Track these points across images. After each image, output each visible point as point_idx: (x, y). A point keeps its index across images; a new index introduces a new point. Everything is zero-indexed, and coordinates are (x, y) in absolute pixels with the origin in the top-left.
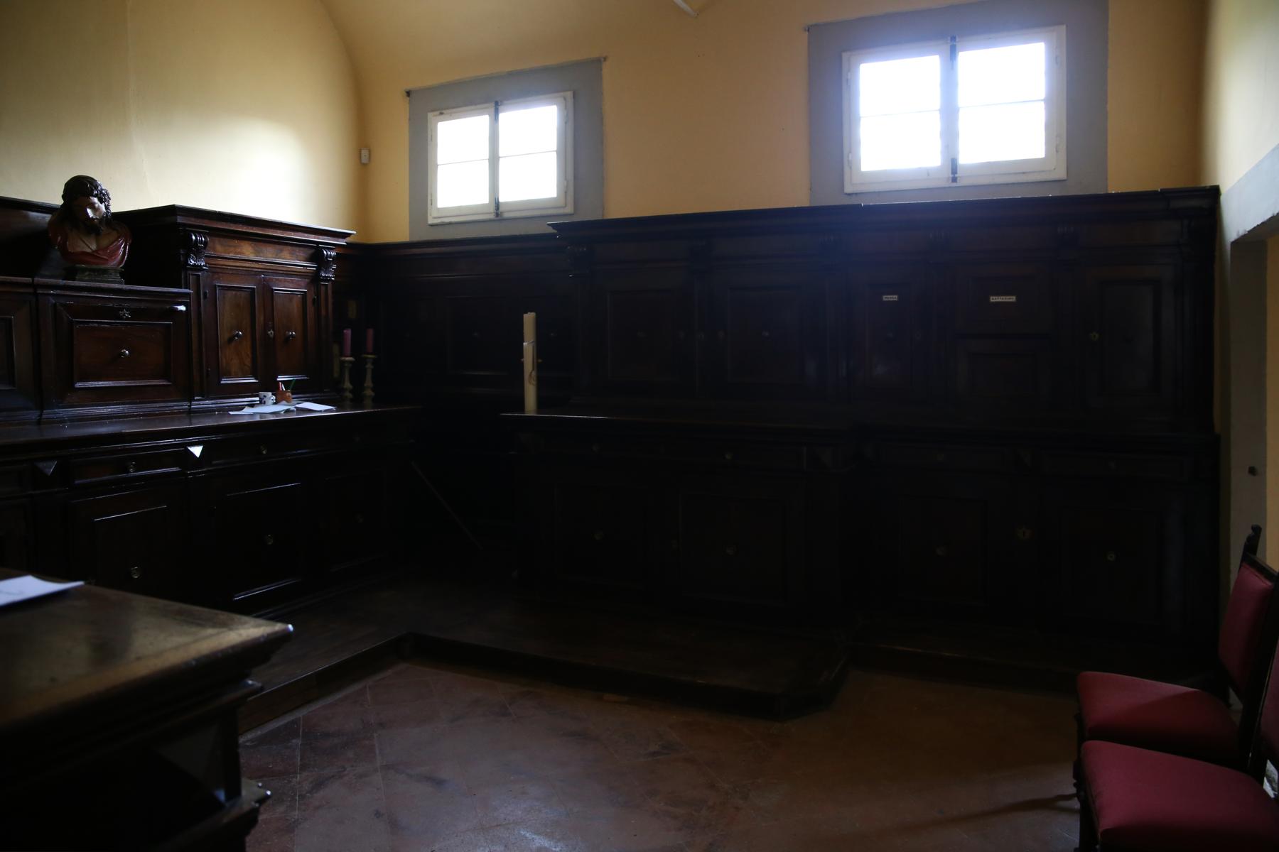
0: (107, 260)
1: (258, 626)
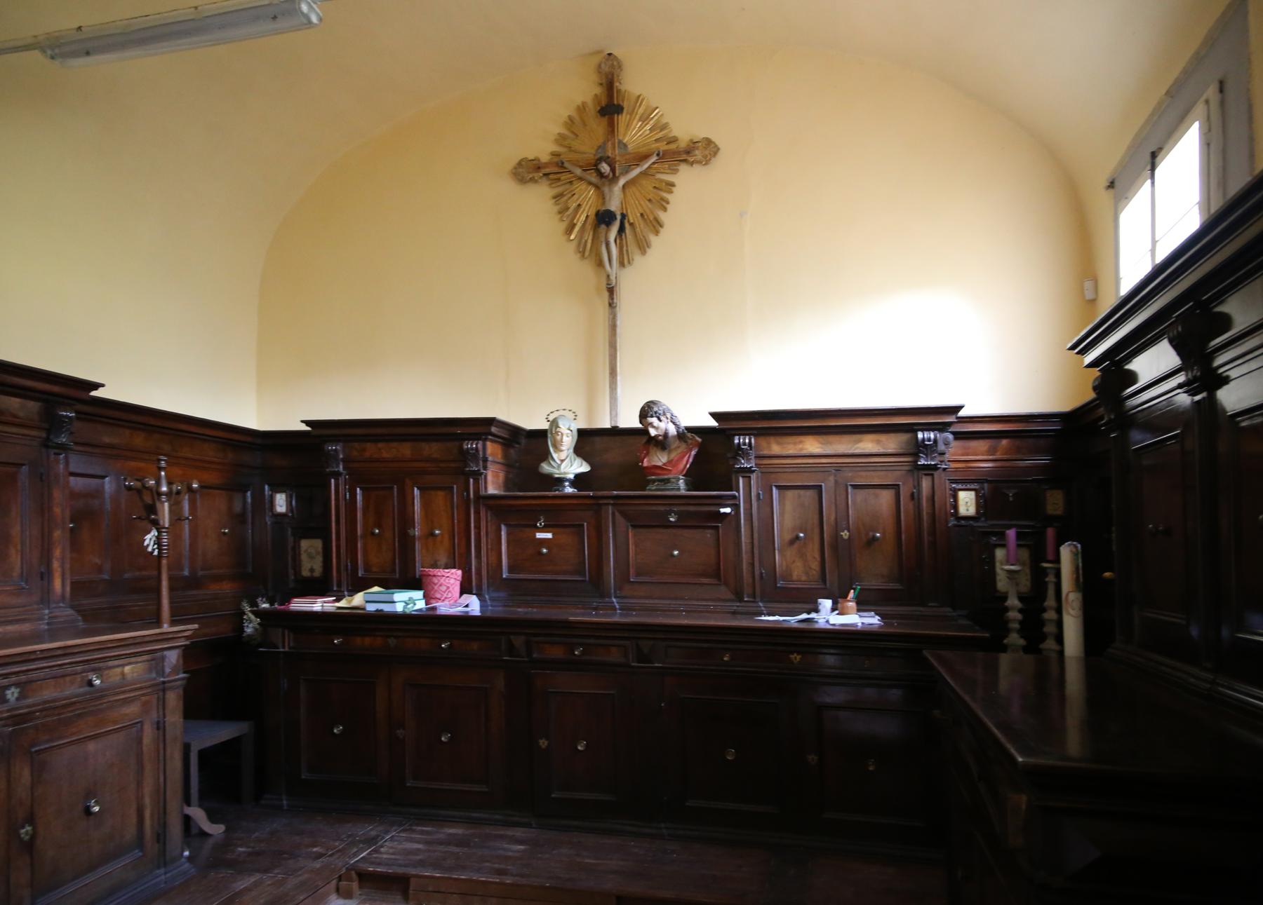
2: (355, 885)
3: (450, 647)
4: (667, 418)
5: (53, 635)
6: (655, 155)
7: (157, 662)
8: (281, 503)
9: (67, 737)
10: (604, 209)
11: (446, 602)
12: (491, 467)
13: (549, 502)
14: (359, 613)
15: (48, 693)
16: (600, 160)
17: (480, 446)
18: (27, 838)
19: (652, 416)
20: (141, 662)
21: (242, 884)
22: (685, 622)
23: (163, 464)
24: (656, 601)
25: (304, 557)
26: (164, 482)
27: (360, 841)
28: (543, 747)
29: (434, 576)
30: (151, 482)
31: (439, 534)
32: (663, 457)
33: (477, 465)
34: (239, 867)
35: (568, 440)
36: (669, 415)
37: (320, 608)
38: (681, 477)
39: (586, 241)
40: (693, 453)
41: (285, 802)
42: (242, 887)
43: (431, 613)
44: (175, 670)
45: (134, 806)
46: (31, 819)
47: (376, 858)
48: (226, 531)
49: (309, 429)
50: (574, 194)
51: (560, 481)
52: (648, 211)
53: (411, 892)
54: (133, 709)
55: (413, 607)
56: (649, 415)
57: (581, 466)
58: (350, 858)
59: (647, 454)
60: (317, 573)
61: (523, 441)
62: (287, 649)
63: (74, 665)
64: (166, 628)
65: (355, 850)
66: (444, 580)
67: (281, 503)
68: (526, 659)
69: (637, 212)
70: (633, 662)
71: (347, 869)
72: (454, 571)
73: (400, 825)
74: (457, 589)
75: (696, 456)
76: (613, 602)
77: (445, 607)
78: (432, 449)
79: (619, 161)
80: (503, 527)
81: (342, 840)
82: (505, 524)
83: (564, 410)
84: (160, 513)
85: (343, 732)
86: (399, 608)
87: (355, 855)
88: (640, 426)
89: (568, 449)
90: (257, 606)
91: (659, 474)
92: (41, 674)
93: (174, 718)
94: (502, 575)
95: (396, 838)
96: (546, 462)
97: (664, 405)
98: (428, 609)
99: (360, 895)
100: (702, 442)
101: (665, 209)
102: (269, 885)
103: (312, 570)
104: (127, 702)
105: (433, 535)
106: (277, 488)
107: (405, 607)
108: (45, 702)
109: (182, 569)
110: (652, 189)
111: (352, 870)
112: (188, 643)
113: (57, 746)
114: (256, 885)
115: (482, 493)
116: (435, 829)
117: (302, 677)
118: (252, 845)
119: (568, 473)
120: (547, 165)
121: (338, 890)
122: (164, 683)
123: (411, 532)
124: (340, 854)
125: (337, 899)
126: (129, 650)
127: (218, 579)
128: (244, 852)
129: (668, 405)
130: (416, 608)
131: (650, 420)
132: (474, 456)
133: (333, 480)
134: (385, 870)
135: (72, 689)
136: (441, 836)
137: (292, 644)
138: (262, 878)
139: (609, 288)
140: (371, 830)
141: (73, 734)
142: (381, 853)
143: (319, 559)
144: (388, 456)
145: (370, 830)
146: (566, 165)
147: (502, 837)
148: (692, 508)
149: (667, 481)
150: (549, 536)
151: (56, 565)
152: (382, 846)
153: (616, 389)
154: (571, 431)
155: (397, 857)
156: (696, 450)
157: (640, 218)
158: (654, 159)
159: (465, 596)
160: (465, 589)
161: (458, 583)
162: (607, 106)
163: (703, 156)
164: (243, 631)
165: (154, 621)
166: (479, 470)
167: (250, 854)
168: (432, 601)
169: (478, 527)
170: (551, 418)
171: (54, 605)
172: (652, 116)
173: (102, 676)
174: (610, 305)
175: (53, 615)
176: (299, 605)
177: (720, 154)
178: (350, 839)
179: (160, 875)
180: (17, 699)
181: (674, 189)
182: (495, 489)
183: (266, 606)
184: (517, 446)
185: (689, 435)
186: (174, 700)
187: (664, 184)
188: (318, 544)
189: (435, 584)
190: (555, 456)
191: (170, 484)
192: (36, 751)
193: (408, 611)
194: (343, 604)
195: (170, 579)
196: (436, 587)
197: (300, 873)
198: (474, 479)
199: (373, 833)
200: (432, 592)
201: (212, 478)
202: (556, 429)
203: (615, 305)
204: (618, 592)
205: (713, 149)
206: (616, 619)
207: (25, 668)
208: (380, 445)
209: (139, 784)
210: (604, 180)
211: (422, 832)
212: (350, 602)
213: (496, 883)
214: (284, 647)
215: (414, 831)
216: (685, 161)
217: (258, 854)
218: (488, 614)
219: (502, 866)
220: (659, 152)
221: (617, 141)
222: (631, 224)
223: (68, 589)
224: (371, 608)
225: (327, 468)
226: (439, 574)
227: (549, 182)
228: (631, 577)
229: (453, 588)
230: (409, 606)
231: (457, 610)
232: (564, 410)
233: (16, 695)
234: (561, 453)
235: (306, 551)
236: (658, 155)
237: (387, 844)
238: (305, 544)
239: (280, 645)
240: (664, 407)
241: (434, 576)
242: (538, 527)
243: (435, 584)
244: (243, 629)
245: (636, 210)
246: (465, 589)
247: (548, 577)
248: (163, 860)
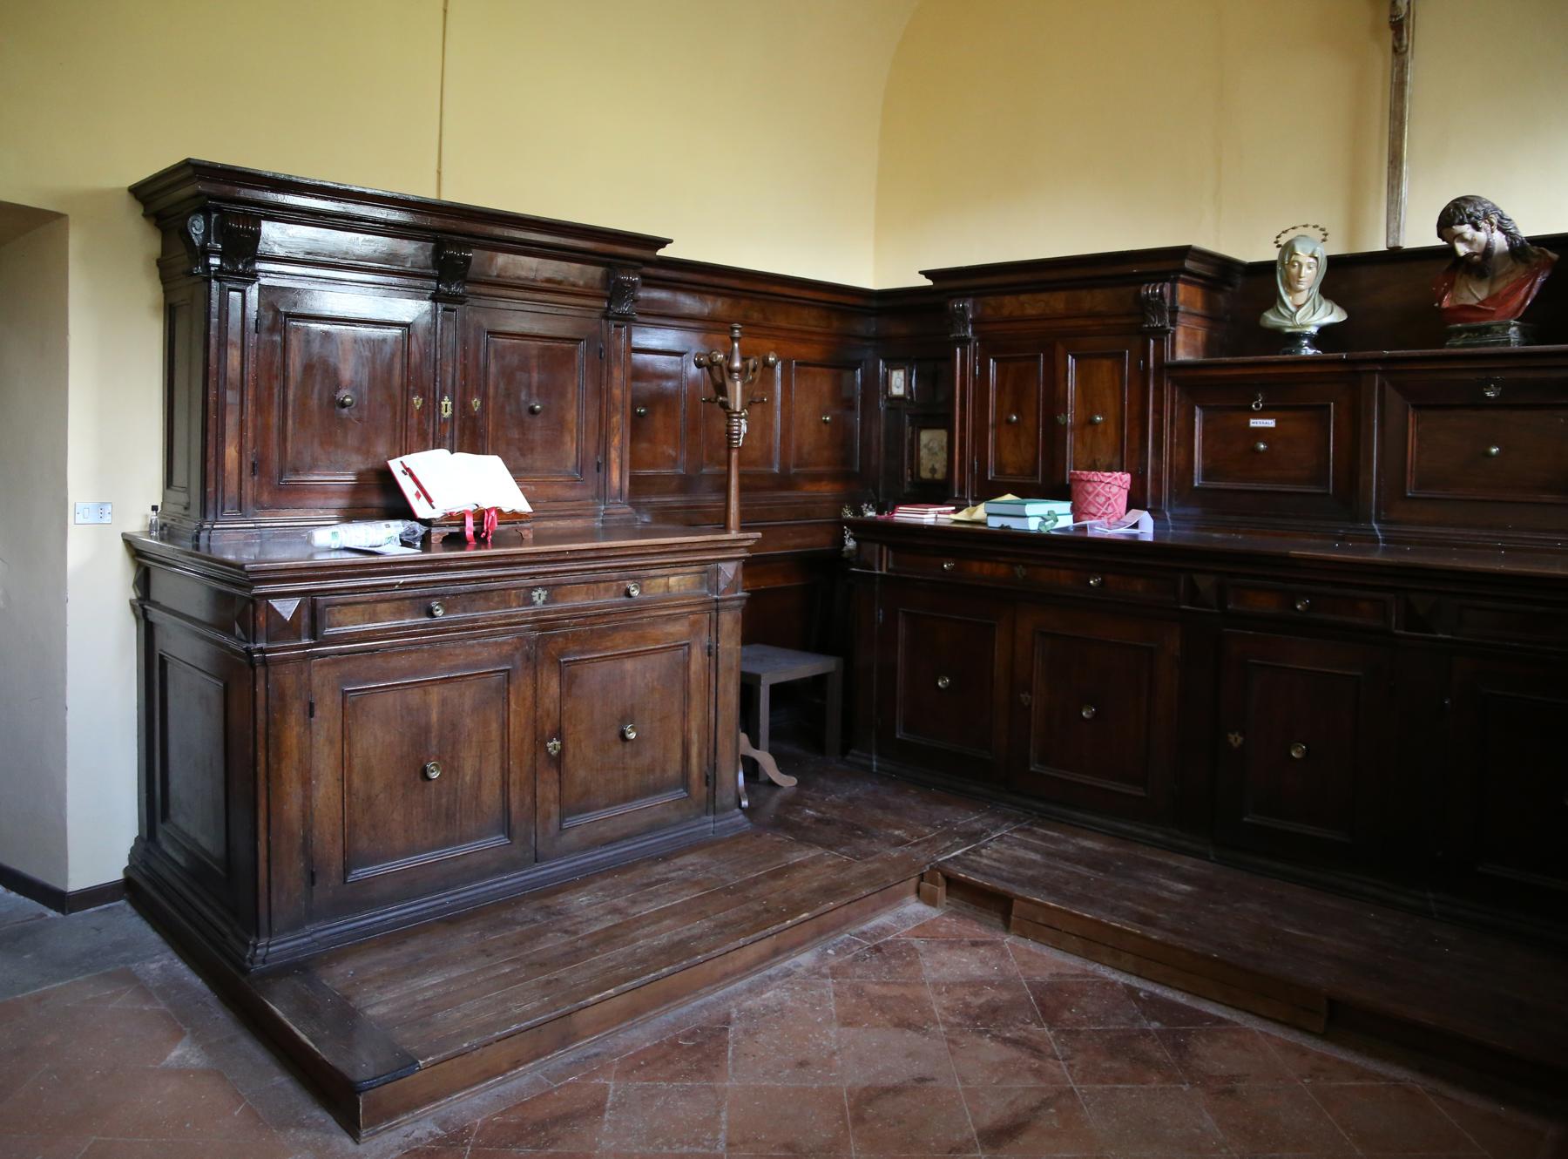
0: (1493, 311)
1: (545, 529)
2: (941, 891)
3: (1102, 584)
4: (1492, 224)
5: (608, 533)
7: (709, 575)
8: (898, 383)
9: (600, 651)
11: (1105, 519)
12: (1182, 321)
13: (1272, 371)
14: (980, 530)
15: (580, 600)
17: (1167, 289)
18: (554, 752)
19: (1462, 223)
20: (688, 574)
21: (797, 856)
22: (1502, 567)
23: (737, 333)
24: (1452, 531)
25: (924, 453)
26: (737, 356)
27: (958, 834)
28: (1235, 745)
29: (1089, 481)
30: (719, 356)
31: (1100, 422)
32: (1479, 291)
33: (1161, 319)
34: (802, 835)
35: (1310, 275)
36: (1495, 219)
37: (933, 520)
38: (1513, 322)
40: (1540, 280)
41: (875, 763)
42: (798, 860)
43: (1081, 534)
44: (732, 586)
45: (678, 740)
46: (559, 734)
47: (972, 861)
48: (828, 419)
49: (929, 283)
51: (1295, 338)
53: (1013, 918)
54: (679, 629)
55: (1053, 525)
56: (1457, 221)
58: (939, 854)
59: (1451, 286)
60: (939, 476)
61: (1239, 281)
62: (884, 572)
63: (609, 570)
64: (734, 534)
65: (948, 844)
66: (1103, 488)
67: (898, 383)
68: (1216, 611)
70: (1396, 628)
71: (931, 867)
72: (1117, 474)
73: (1017, 821)
74: (1122, 501)
75: (1544, 284)
76: (1374, 530)
77: (1101, 526)
78: (1096, 300)
80: (1197, 411)
81: (935, 827)
82: (1199, 406)
83: (1305, 226)
84: (730, 392)
85: (949, 688)
86: (1033, 525)
87: (947, 851)
88: (1439, 242)
89: (1310, 289)
90: (862, 514)
91: (1479, 320)
92: (571, 578)
93: (730, 644)
94: (1193, 483)
95: (1005, 838)
96: (1271, 310)
97: (1487, 202)
98: (1077, 529)
99: (947, 904)
100: (1559, 260)
102: (829, 866)
103: (933, 470)
104: (670, 619)
105: (1092, 422)
106: (893, 364)
107: (1040, 524)
108: (575, 609)
109: (771, 465)
111: (938, 870)
112: (748, 555)
113: (588, 659)
114: (813, 862)
115: (1168, 359)
116: (1062, 836)
117: (902, 609)
118: (823, 809)
119: (1308, 326)
121: (918, 891)
122: (717, 600)
123: (1061, 419)
124: (926, 845)
125: (917, 902)
126: (677, 558)
127: (817, 478)
128: (812, 816)
129: (1495, 202)
130: (1058, 526)
131: (1458, 229)
132: (1157, 305)
133: (958, 350)
134: (980, 881)
135: (607, 598)
136: (1070, 848)
137: (891, 566)
138: (823, 854)
139: (1396, 22)
140: (976, 821)
141: (606, 649)
142: (981, 856)
143: (943, 456)
144: (1034, 312)
145: (973, 820)
147: (1159, 866)
148: (1530, 375)
149: (1487, 330)
150: (1271, 423)
151: (614, 455)
152: (984, 847)
154: (1316, 258)
155: (1003, 866)
156: (1546, 275)
159: (1133, 511)
160: (1134, 502)
161: (1126, 492)
164: (844, 545)
165: (722, 526)
166: (1163, 327)
167: (818, 820)
168: (1084, 517)
169: (1159, 411)
170: (1283, 241)
171: (611, 501)
173: (641, 586)
174: (1395, 50)
175: (608, 512)
176: (906, 515)
178: (945, 828)
179: (709, 823)
180: (544, 602)
182: (1188, 354)
183: (871, 514)
184: (1229, 289)
185: (1534, 250)
186: (729, 622)
188: (941, 435)
189: (1089, 494)
190: (1287, 299)
191: (744, 359)
192: (565, 662)
193: (1044, 530)
194: (962, 516)
195: (741, 476)
196: (1090, 498)
197: (870, 859)
198: (961, 348)
199: (978, 826)
200: (1085, 505)
201: (812, 352)
202: (1290, 257)
204: (1383, 513)
206: (1377, 557)
207: (553, 569)
208: (1023, 298)
209: (685, 716)
211: (1044, 838)
212: (972, 514)
213: (1135, 934)
214: (881, 569)
215: (1033, 833)
217: (829, 822)
218: (1168, 540)
219: (1151, 912)
223: (627, 483)
224: (994, 523)
225: (952, 333)
226: (1096, 479)
228: (1408, 490)
229: (1116, 500)
230: (1047, 523)
231: (1120, 532)
232: (1305, 226)
233: (543, 598)
234: (1298, 295)
235: (925, 446)
237: (992, 844)
238: (925, 436)
239: (877, 566)
240: (1486, 205)
241: (1089, 481)
242: (1253, 410)
243: (1089, 494)
244: (844, 542)
246: (1134, 502)
247: (1268, 487)
248: (711, 805)
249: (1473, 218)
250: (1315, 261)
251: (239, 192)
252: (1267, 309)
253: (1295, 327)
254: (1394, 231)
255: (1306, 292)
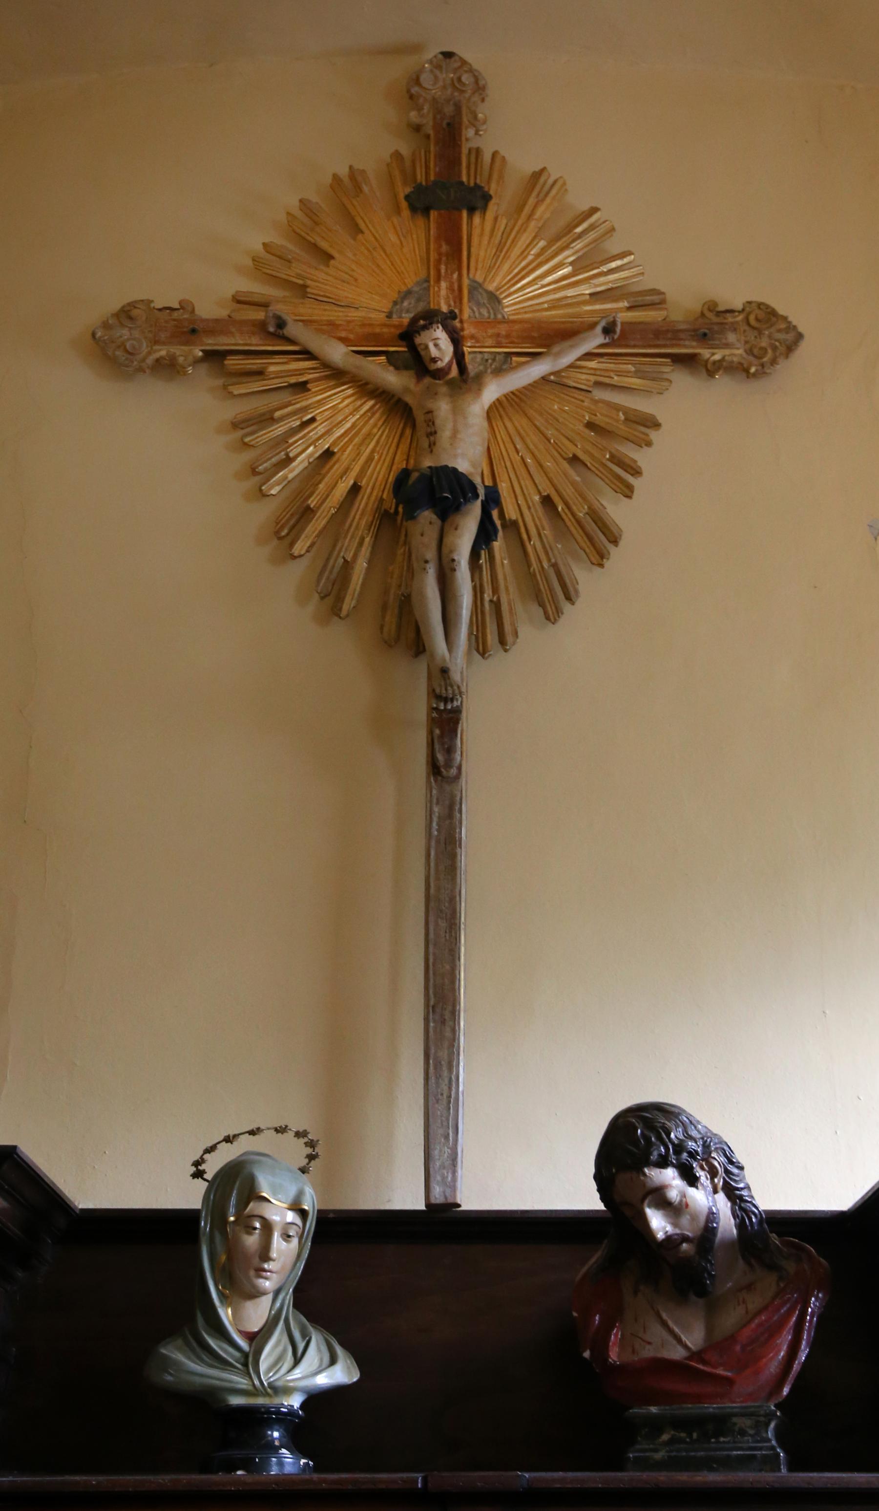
6: (599, 329)
10: (428, 462)
16: (430, 318)
19: (663, 1163)
36: (718, 1160)
39: (347, 566)
50: (313, 420)
52: (569, 492)
56: (654, 1157)
57: (333, 1361)
69: (531, 490)
75: (823, 1318)
79: (472, 337)
91: (699, 1398)
101: (628, 491)
110: (580, 427)
119: (287, 1391)
120: (217, 327)
146: (293, 330)
153: (452, 1064)
157: (540, 510)
158: (594, 341)
162: (435, 183)
163: (750, 352)
170: (213, 1166)
172: (579, 230)
174: (435, 769)
177: (804, 347)
181: (654, 435)
187: (622, 416)
203: (453, 771)
205: (781, 336)
210: (427, 380)
216: (687, 361)
220: (614, 323)
221: (466, 282)
222: (512, 526)
227: (219, 382)
236: (608, 331)
245: (527, 483)
249: (685, 1155)
250: (299, 1222)
251: (787, 1388)
252: (167, 1334)
253: (254, 1392)
254: (443, 1167)
255: (270, 1297)
